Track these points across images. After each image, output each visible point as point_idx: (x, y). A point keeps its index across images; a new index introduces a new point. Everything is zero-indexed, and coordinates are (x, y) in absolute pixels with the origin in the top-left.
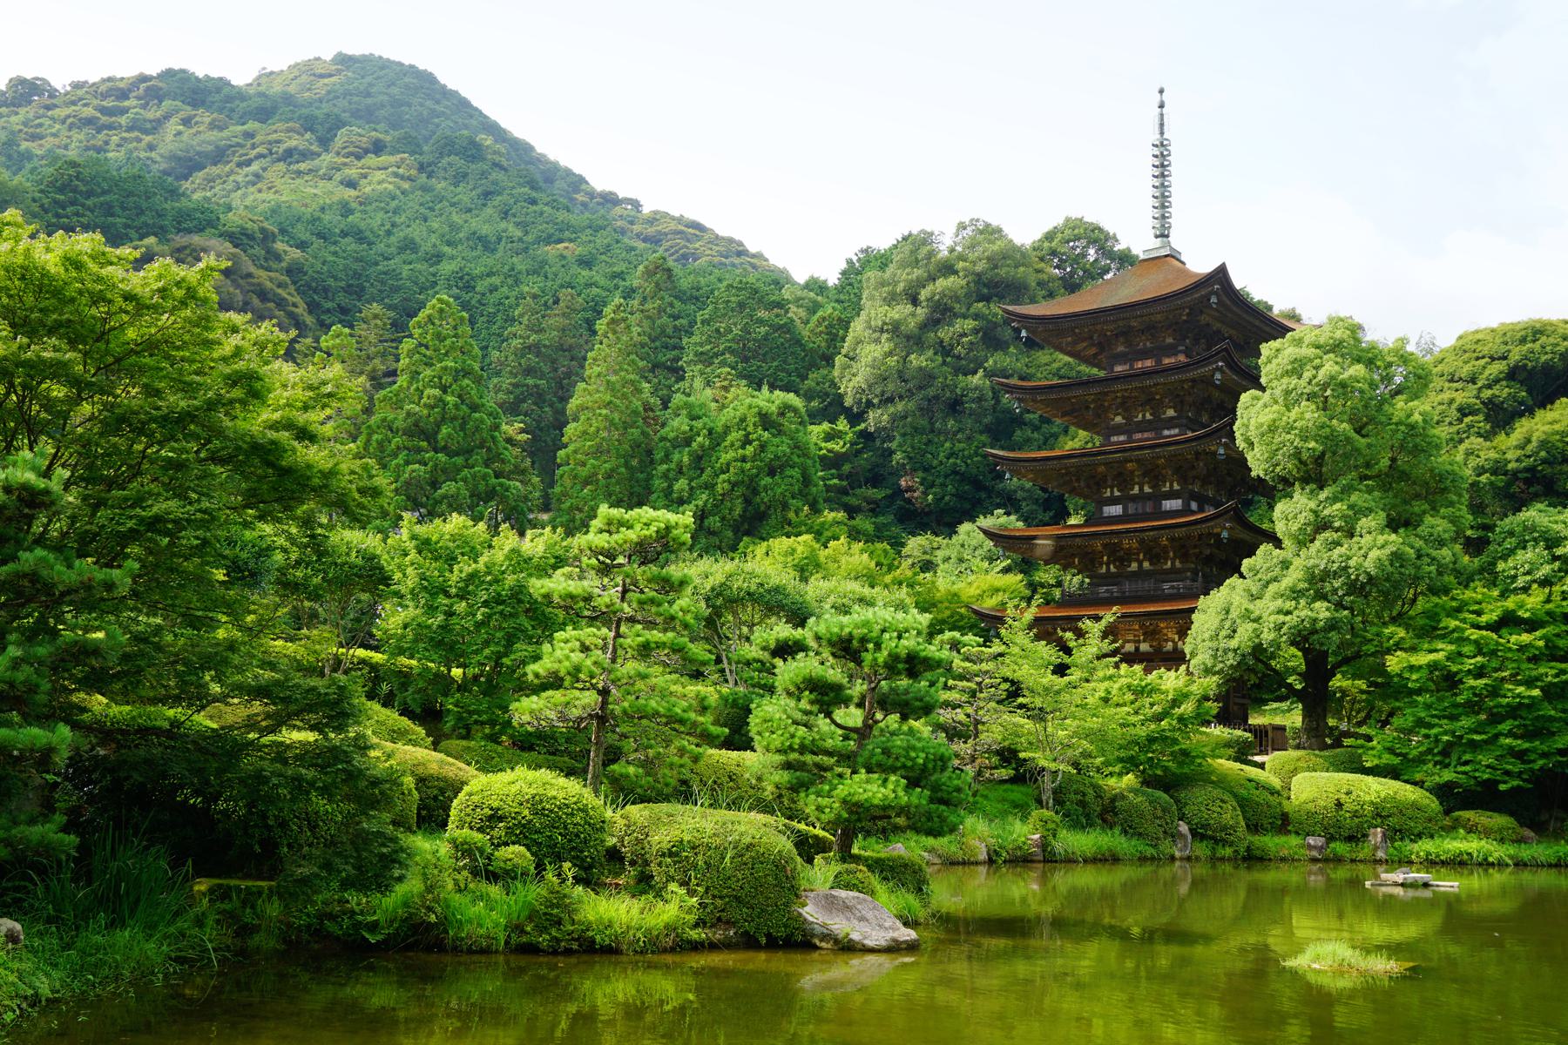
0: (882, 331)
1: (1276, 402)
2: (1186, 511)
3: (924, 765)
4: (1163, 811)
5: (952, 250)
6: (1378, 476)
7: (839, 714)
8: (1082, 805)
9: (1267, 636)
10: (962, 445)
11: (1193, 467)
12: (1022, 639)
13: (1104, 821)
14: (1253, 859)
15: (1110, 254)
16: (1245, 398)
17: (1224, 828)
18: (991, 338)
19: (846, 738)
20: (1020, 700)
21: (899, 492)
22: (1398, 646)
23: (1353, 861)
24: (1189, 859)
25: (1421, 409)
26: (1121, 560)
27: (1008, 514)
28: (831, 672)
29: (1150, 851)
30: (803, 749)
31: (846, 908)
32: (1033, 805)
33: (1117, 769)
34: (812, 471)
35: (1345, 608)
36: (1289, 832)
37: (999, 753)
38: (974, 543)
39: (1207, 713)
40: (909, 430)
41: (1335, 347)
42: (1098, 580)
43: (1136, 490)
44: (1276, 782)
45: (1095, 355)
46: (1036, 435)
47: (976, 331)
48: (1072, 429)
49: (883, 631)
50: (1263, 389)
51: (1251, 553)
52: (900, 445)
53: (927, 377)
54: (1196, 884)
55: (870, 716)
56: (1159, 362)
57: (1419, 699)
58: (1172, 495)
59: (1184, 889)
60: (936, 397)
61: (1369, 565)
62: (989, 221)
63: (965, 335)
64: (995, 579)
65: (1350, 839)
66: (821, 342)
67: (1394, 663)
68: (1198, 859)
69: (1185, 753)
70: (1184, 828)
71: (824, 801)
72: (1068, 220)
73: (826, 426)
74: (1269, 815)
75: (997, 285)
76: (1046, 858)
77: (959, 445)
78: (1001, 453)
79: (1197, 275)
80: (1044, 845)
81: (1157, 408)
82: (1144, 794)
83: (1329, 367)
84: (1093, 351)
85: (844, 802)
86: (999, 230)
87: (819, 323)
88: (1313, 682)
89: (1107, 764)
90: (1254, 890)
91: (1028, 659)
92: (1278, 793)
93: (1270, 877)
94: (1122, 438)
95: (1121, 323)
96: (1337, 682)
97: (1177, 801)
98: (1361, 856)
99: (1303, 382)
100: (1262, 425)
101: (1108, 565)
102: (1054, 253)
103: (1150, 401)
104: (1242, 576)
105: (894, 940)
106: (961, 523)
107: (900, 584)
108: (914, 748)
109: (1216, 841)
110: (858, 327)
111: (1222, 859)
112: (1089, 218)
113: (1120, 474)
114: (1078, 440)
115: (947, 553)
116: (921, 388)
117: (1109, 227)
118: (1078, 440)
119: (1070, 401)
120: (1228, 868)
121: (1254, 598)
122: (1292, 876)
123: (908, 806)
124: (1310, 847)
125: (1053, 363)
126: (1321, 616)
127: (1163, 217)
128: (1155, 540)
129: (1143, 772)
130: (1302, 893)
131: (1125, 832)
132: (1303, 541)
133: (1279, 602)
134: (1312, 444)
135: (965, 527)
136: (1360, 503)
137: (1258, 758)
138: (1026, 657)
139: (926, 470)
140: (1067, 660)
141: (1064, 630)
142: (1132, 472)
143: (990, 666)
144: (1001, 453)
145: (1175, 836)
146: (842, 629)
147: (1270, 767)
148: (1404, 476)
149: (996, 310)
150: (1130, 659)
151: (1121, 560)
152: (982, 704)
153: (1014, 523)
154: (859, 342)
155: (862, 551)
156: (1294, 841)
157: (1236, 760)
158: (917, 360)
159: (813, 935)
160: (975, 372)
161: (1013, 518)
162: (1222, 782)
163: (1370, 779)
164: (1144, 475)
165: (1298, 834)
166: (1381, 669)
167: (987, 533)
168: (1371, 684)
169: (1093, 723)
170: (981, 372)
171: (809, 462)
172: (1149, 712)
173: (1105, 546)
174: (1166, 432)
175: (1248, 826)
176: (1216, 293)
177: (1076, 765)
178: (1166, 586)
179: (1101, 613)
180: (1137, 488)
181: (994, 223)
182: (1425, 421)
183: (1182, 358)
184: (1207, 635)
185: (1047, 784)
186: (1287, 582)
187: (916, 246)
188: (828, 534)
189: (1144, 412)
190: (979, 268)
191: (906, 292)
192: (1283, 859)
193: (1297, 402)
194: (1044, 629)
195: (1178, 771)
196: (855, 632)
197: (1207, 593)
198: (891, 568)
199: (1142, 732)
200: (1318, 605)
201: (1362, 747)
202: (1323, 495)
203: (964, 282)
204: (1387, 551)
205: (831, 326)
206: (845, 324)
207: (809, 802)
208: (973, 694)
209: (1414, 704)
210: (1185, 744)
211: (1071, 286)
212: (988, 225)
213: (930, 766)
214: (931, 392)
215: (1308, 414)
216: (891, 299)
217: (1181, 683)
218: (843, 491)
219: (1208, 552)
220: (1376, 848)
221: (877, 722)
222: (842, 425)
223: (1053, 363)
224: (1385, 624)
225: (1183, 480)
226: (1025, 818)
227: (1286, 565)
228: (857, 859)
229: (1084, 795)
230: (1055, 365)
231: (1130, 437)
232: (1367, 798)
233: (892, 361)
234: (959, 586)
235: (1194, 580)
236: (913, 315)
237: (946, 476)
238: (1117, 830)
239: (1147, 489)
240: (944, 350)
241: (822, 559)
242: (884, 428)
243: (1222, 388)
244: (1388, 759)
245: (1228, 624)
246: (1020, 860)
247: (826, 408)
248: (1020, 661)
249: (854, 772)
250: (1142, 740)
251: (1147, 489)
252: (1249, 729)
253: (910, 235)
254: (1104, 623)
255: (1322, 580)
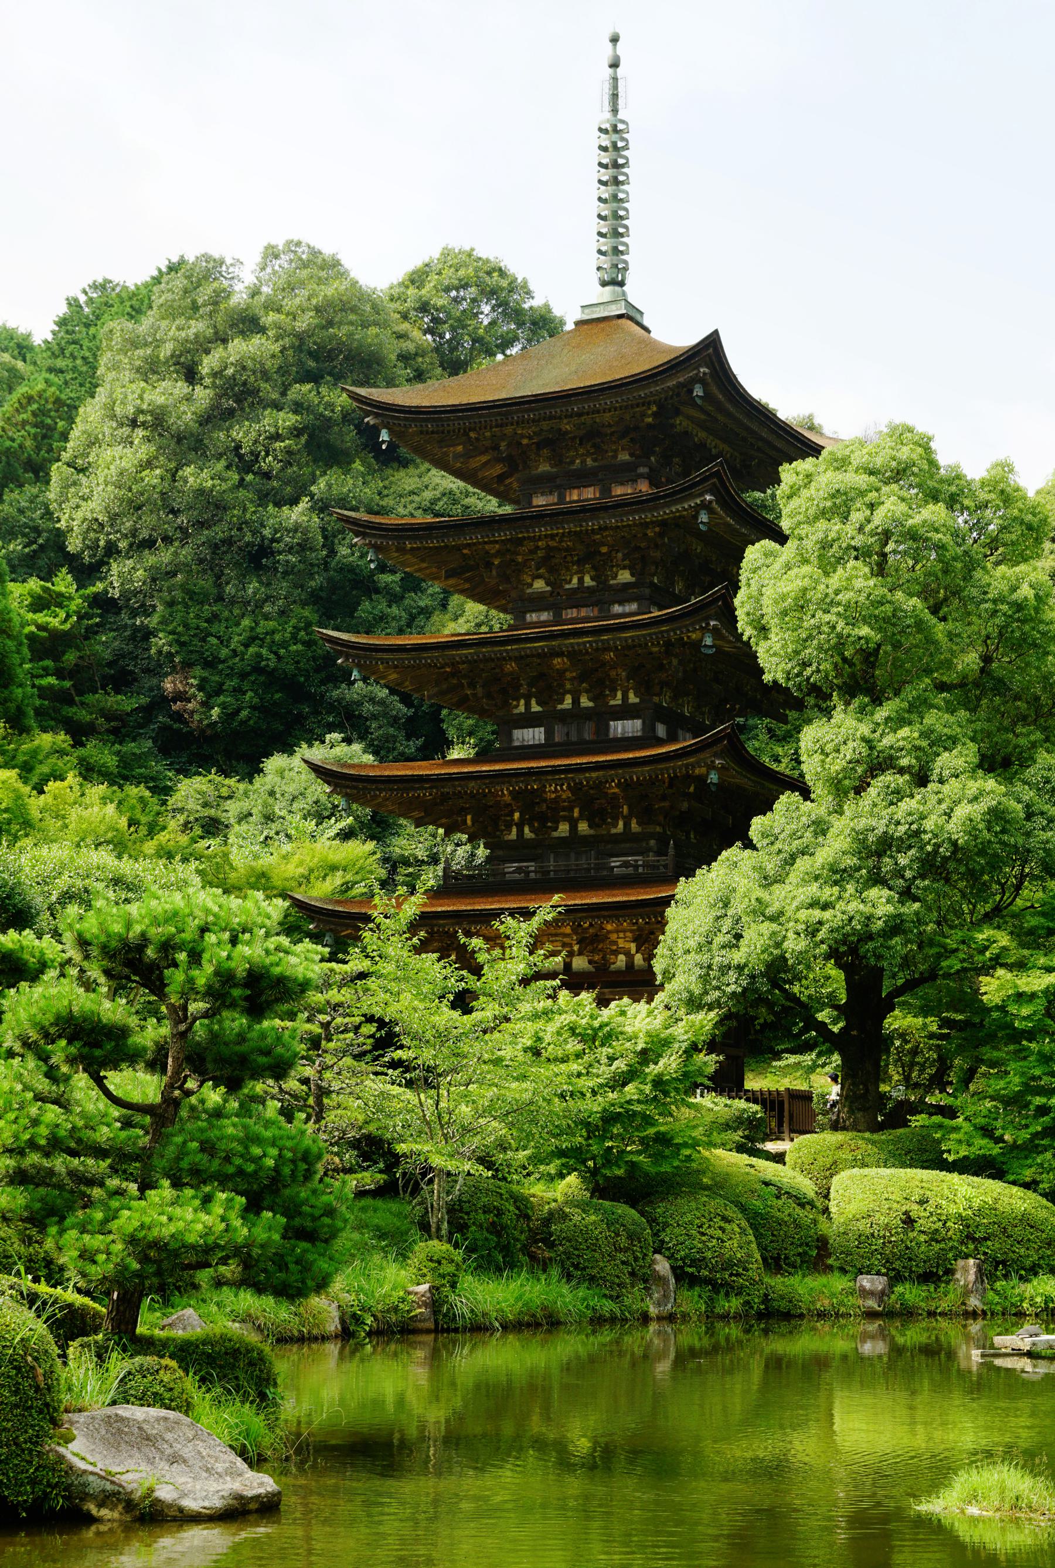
0: (134, 423)
1: (806, 561)
2: (648, 739)
3: (276, 1169)
4: (630, 1237)
5: (255, 293)
6: (962, 685)
7: (118, 1080)
8: (498, 1233)
9: (794, 945)
10: (272, 624)
11: (661, 667)
12: (397, 949)
13: (533, 1257)
14: (777, 1315)
15: (517, 315)
16: (753, 553)
17: (728, 1265)
18: (320, 445)
19: (127, 1124)
20: (399, 1054)
21: (161, 702)
22: (997, 962)
23: (932, 1314)
24: (671, 1318)
25: (1033, 577)
26: (543, 818)
27: (348, 741)
28: (107, 1004)
29: (608, 1307)
30: (55, 1145)
31: (146, 1440)
32: (415, 1233)
33: (552, 1169)
34: (16, 659)
35: (916, 899)
36: (830, 1268)
37: (355, 1144)
38: (291, 789)
39: (700, 1072)
40: (178, 594)
41: (899, 474)
42: (500, 851)
43: (568, 702)
44: (807, 1187)
45: (501, 478)
46: (395, 610)
47: (296, 432)
48: (456, 599)
49: (204, 930)
50: (781, 539)
51: (766, 807)
52: (164, 622)
53: (212, 506)
54: (683, 1359)
55: (177, 1082)
56: (606, 491)
57: (1033, 1045)
58: (625, 712)
59: (663, 1367)
60: (229, 542)
61: (955, 828)
62: (318, 245)
63: (277, 437)
64: (325, 846)
65: (927, 1278)
66: (24, 439)
67: (994, 988)
68: (685, 1317)
69: (663, 1139)
70: (663, 1266)
71: (96, 1241)
72: (446, 253)
73: (34, 584)
74: (798, 1243)
75: (331, 356)
76: (439, 1327)
77: (265, 622)
78: (344, 636)
79: (676, 348)
80: (435, 1302)
81: (602, 568)
82: (597, 1210)
83: (891, 506)
84: (498, 469)
85: (132, 1240)
86: (336, 264)
87: (21, 407)
88: (861, 1024)
89: (537, 1159)
90: (776, 1365)
91: (405, 982)
92: (811, 1204)
93: (802, 1344)
94: (544, 616)
95: (545, 425)
96: (897, 1021)
97: (652, 1221)
98: (944, 1305)
99: (850, 529)
100: (784, 597)
101: (520, 827)
102: (424, 307)
103: (591, 557)
104: (749, 845)
105: (239, 1497)
106: (268, 755)
107: (170, 856)
108: (257, 1140)
109: (716, 1287)
110: (91, 415)
111: (725, 1317)
112: (486, 251)
113: (542, 675)
114: (467, 618)
115: (244, 805)
116: (201, 525)
117: (518, 268)
118: (467, 618)
119: (452, 552)
120: (734, 1331)
121: (768, 881)
122: (834, 1342)
123: (249, 1244)
124: (864, 1293)
125: (429, 488)
126: (880, 912)
127: (616, 251)
128: (599, 785)
129: (595, 1172)
130: (853, 1367)
131: (569, 1277)
132: (850, 787)
133: (813, 889)
134: (865, 631)
135: (275, 763)
136: (938, 727)
137: (771, 1147)
138: (407, 979)
139: (210, 664)
140: (472, 983)
141: (468, 934)
142: (561, 673)
143: (344, 995)
144: (344, 636)
145: (647, 1279)
146: (128, 926)
147: (792, 1162)
148: (1000, 686)
149: (337, 398)
150: (575, 983)
151: (543, 818)
152: (329, 1059)
153: (355, 755)
154: (93, 442)
155: (104, 800)
156: (839, 1283)
157: (740, 1149)
158: (195, 477)
159: (85, 1496)
160: (294, 502)
161: (357, 747)
162: (720, 1185)
163: (954, 1178)
164: (582, 678)
165: (843, 1271)
166: (971, 1001)
167: (318, 770)
168: (945, 1023)
169: (518, 1091)
170: (304, 504)
171: (10, 644)
172: (605, 1072)
173: (515, 795)
174: (617, 609)
175: (764, 1259)
176: (702, 381)
177: (485, 1161)
178: (615, 862)
179: (532, 905)
180: (568, 700)
181: (328, 250)
182: (1037, 596)
183: (644, 487)
184: (692, 943)
185: (436, 1193)
186: (824, 855)
187: (193, 283)
188: (45, 769)
189: (581, 572)
190: (303, 323)
191: (175, 359)
192: (822, 1315)
193: (840, 560)
194: (436, 934)
195: (653, 1170)
196: (153, 931)
197: (690, 874)
198: (153, 829)
199: (594, 1106)
200: (874, 893)
201: (940, 1126)
202: (881, 714)
203: (276, 348)
204: (982, 806)
205: (41, 412)
206: (69, 410)
207: (66, 1245)
208: (315, 1043)
209: (1021, 1055)
210: (663, 1125)
211: (455, 367)
212: (315, 253)
213: (287, 1170)
214: (219, 532)
215: (857, 580)
216: (150, 370)
217: (657, 1022)
218: (63, 698)
219: (685, 806)
220: (967, 1293)
221: (188, 1093)
222: (64, 583)
223: (429, 488)
224: (977, 925)
225: (645, 688)
226: (403, 1256)
227: (821, 828)
228: (146, 1345)
229: (500, 1213)
230: (428, 495)
231: (558, 615)
232: (953, 1209)
233: (153, 477)
234: (267, 861)
235: (661, 852)
236: (188, 398)
237: (243, 676)
238: (555, 1272)
239: (585, 702)
240: (243, 462)
241: (35, 814)
242: (135, 593)
243: (708, 538)
244: (982, 1146)
245: (727, 924)
246: (394, 1330)
247: (34, 555)
248: (394, 987)
249: (145, 1186)
250: (595, 1119)
251: (585, 702)
252: (753, 1097)
253: (182, 261)
254: (536, 922)
255: (880, 854)
